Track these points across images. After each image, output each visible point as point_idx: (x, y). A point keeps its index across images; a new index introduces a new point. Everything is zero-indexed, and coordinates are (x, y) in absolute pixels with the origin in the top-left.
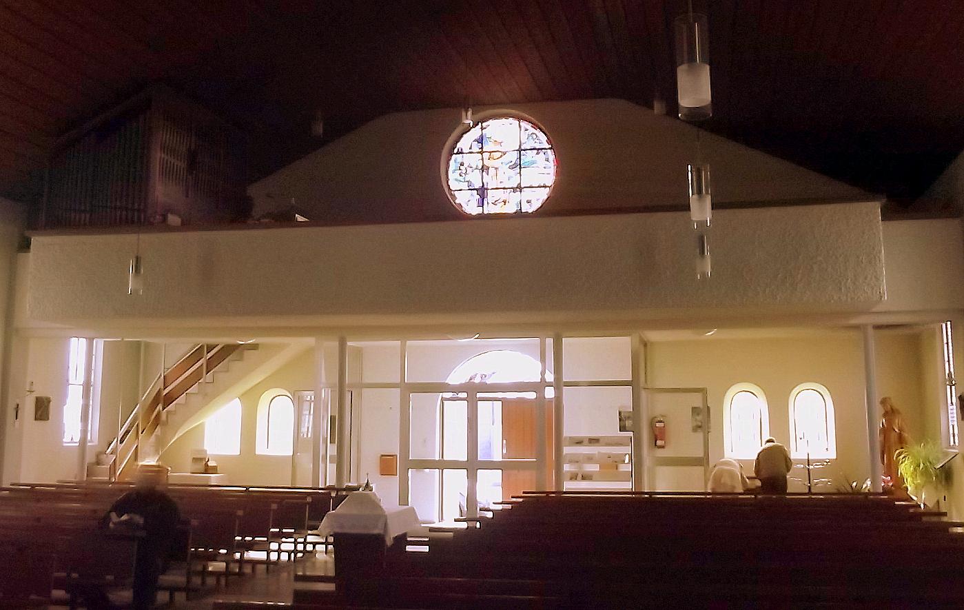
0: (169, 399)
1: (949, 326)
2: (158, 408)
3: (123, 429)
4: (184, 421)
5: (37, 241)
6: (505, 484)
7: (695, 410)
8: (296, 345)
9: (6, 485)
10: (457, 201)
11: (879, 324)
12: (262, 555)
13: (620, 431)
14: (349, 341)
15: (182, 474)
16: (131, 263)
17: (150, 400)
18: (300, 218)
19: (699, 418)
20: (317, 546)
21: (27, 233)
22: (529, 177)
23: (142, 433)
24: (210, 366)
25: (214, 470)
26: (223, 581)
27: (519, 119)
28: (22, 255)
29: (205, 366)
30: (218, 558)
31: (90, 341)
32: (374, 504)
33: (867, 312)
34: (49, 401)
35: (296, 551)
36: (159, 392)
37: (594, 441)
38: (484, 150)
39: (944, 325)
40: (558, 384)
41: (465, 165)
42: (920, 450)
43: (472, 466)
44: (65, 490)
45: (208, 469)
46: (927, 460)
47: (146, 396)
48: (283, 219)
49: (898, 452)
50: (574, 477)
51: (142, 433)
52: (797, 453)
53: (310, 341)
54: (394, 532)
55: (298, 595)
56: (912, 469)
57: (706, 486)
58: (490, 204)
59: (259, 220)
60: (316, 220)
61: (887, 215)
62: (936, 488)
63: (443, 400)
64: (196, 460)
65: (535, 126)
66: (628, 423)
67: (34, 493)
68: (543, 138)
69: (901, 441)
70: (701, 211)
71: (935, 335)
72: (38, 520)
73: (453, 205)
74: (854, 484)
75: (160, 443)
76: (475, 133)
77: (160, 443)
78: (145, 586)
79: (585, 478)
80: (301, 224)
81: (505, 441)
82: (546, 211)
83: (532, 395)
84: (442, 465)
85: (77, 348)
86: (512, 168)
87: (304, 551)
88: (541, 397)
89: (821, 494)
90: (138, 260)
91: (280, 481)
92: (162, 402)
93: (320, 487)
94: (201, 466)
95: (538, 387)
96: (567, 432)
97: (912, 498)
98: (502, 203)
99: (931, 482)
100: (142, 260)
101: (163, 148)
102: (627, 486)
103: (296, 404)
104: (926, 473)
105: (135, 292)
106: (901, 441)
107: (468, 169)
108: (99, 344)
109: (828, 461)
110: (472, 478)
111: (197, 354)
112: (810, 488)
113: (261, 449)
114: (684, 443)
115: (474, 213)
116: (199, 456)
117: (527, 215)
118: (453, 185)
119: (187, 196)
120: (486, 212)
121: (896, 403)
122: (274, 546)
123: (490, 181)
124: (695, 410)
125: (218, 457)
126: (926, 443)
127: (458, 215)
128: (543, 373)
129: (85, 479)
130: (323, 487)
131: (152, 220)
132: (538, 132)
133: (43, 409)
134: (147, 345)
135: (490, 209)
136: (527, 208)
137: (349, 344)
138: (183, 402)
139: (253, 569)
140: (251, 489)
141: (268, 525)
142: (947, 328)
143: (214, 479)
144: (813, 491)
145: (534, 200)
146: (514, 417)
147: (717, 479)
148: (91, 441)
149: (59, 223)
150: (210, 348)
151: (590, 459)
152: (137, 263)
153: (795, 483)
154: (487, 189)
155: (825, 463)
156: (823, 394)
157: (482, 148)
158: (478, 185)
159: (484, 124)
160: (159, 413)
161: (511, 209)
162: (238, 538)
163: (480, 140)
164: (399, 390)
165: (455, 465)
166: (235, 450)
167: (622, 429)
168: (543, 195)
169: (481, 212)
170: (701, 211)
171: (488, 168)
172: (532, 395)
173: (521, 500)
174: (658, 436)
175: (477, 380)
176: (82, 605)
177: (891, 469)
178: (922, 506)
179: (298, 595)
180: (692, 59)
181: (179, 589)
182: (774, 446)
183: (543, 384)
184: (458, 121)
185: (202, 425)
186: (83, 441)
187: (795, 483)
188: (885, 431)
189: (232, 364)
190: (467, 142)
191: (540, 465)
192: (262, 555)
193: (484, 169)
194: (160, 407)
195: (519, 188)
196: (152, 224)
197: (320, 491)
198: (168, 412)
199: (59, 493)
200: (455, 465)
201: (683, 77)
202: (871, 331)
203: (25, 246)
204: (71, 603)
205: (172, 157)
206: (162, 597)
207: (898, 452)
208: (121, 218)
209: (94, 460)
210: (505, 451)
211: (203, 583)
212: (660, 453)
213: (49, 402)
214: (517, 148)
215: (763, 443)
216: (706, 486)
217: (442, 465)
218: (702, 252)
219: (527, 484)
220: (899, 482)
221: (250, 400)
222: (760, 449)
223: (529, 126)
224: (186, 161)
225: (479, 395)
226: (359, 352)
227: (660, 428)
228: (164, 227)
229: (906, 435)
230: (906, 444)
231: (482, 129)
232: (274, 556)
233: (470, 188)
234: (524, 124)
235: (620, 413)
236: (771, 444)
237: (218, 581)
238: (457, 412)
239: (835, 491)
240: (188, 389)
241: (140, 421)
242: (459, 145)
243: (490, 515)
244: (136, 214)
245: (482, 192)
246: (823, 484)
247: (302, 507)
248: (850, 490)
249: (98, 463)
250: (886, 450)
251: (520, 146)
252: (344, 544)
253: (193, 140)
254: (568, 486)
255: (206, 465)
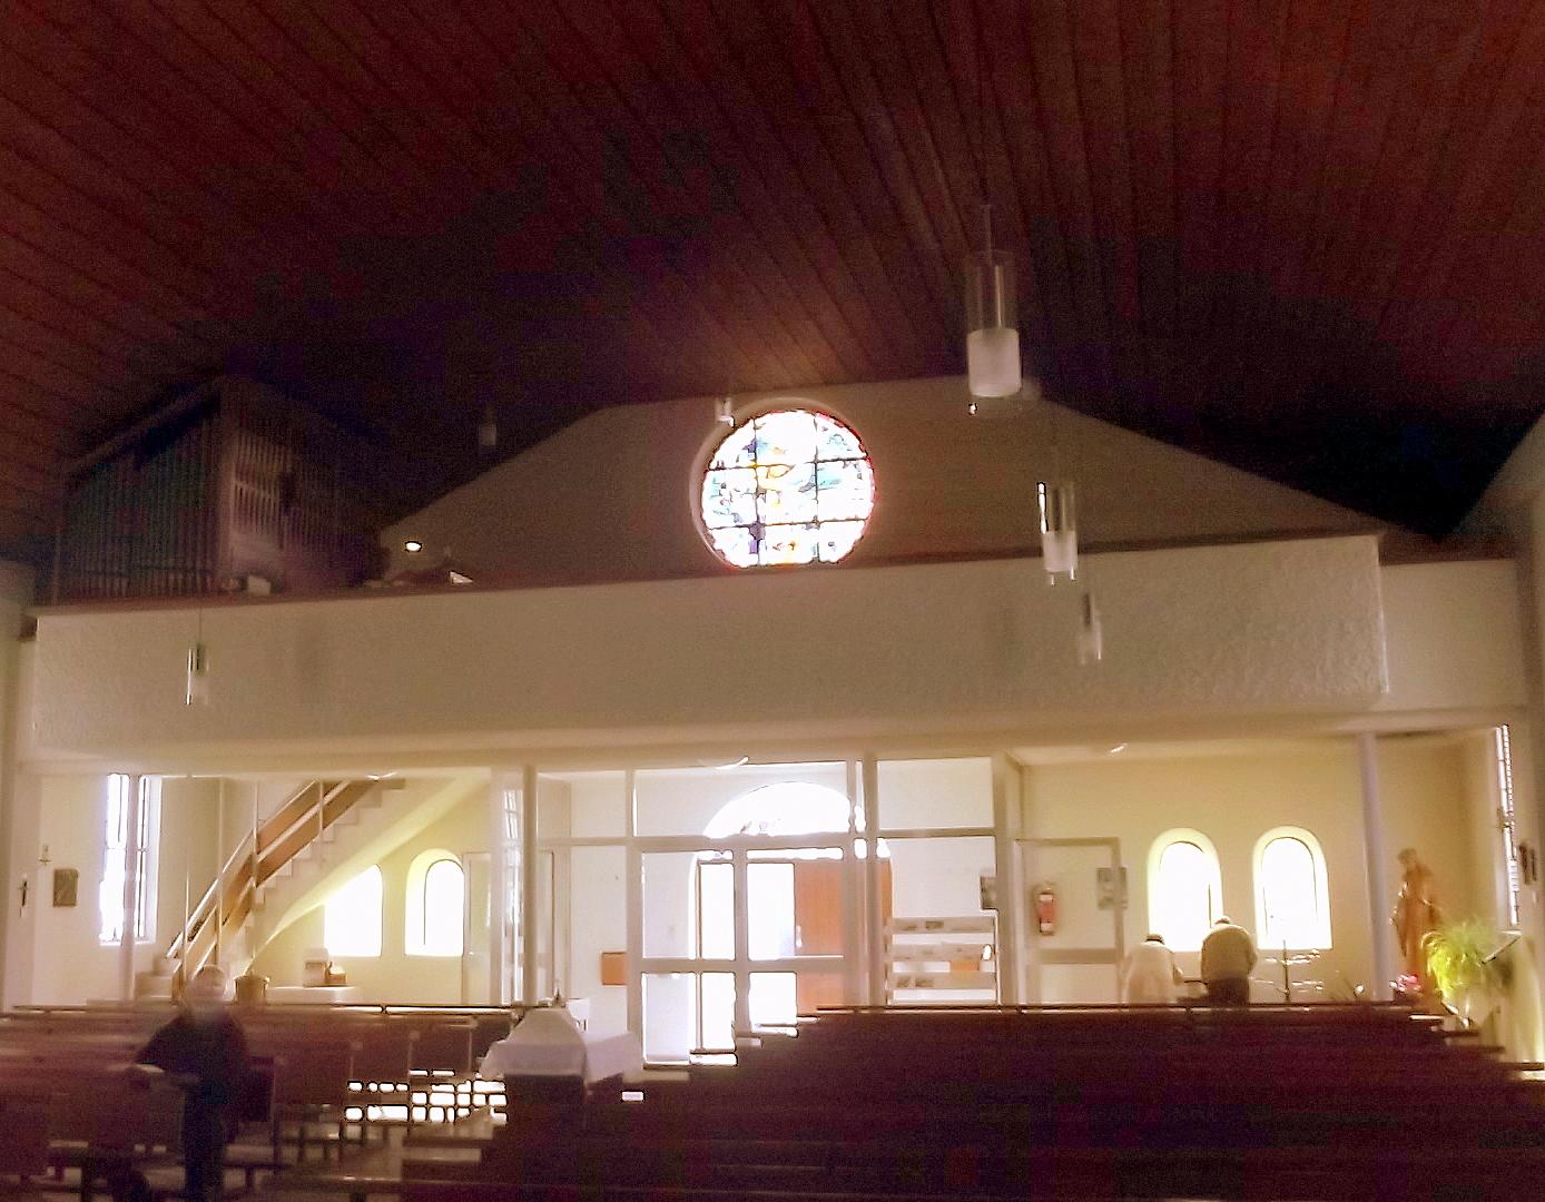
0: (266, 870)
1: (1506, 733)
2: (248, 885)
3: (192, 918)
4: (289, 906)
5: (46, 623)
6: (802, 991)
7: (1103, 875)
8: (464, 779)
9: (7, 1009)
10: (716, 546)
11: (1408, 730)
12: (398, 1113)
13: (984, 909)
14: (541, 771)
15: (288, 987)
16: (191, 655)
17: (236, 872)
18: (457, 579)
19: (1109, 886)
20: (491, 1097)
21: (32, 612)
22: (828, 505)
23: (224, 923)
24: (329, 814)
25: (339, 981)
26: (334, 1154)
27: (814, 411)
28: (25, 647)
29: (321, 815)
30: (321, 1117)
31: (135, 779)
32: (567, 1028)
33: (1363, 713)
34: (75, 875)
35: (456, 1107)
36: (251, 857)
37: (934, 925)
38: (759, 463)
39: (1498, 731)
40: (872, 835)
41: (730, 487)
42: (1461, 932)
43: (741, 968)
44: (101, 1015)
45: (330, 980)
46: (1473, 949)
47: (229, 866)
48: (430, 579)
49: (1425, 936)
50: (903, 983)
51: (224, 923)
52: (1266, 940)
53: (481, 773)
54: (598, 1073)
55: (409, 1168)
56: (1448, 963)
57: (1120, 996)
58: (770, 548)
59: (389, 583)
60: (484, 579)
61: (1388, 557)
62: (1488, 993)
63: (700, 863)
64: (311, 965)
65: (840, 423)
66: (993, 897)
67: (49, 1021)
68: (853, 441)
69: (1433, 918)
70: (1061, 556)
71: (1485, 746)
72: (40, 1060)
73: (709, 551)
74: (1360, 989)
75: (253, 939)
76: (744, 435)
77: (253, 939)
78: (203, 1165)
79: (920, 984)
80: (460, 588)
81: (799, 928)
82: (861, 558)
83: (835, 854)
84: (701, 967)
85: (116, 787)
86: (803, 490)
87: (471, 1106)
88: (850, 857)
89: (1307, 1006)
90: (200, 652)
91: (443, 995)
92: (255, 868)
93: (503, 1003)
94: (320, 976)
95: (843, 841)
96: (898, 912)
97: (1449, 1011)
98: (788, 548)
99: (1479, 984)
100: (207, 651)
101: (241, 474)
102: (987, 996)
103: (467, 869)
104: (1469, 970)
105: (197, 700)
106: (1433, 918)
107: (734, 493)
108: (153, 787)
109: (1315, 952)
110: (742, 987)
111: (309, 798)
112: (1287, 995)
113: (413, 947)
114: (1085, 925)
115: (744, 565)
116: (316, 959)
117: (828, 566)
118: (711, 519)
119: (281, 546)
120: (763, 563)
121: (1424, 857)
122: (419, 1098)
123: (769, 512)
124: (1103, 875)
125: (345, 961)
126: (1472, 921)
127: (709, 566)
128: (852, 820)
129: (131, 996)
130: (508, 1004)
131: (223, 586)
132: (844, 432)
133: (65, 889)
134: (230, 785)
135: (768, 557)
136: (831, 555)
137: (541, 775)
138: (289, 873)
139: (385, 1136)
140: (389, 1009)
141: (406, 1066)
142: (1502, 735)
143: (339, 994)
144: (1294, 1000)
145: (839, 542)
146: (812, 888)
147: (1137, 986)
148: (145, 938)
149: (82, 594)
150: (329, 787)
151: (929, 954)
152: (198, 655)
153: (1263, 989)
154: (764, 525)
155: (1312, 956)
156: (1307, 843)
157: (755, 460)
158: (751, 520)
159: (759, 422)
160: (251, 889)
161: (802, 556)
162: (356, 1087)
163: (752, 448)
164: (622, 849)
165: (717, 967)
166: (373, 950)
167: (986, 905)
168: (855, 532)
169: (754, 562)
170: (1061, 556)
171: (765, 493)
172: (835, 854)
173: (813, 1019)
174: (1043, 915)
175: (753, 832)
176: (101, 1191)
177: (1416, 964)
178: (1466, 1022)
179: (409, 1168)
180: (989, 322)
181: (262, 1166)
182: (1227, 929)
183: (853, 834)
184: (709, 420)
185: (318, 912)
186: (128, 937)
187: (1263, 989)
188: (1408, 904)
189: (364, 811)
190: (731, 450)
191: (848, 966)
192: (398, 1113)
193: (760, 493)
194: (252, 882)
195: (816, 523)
196: (221, 592)
197: (503, 1011)
198: (267, 891)
199: (89, 1020)
200: (717, 967)
201: (976, 345)
202: (1371, 744)
203: (28, 631)
204: (85, 1190)
205: (256, 484)
206: (233, 1179)
207: (1425, 936)
208: (112, 591)
209: (149, 968)
210: (799, 943)
211: (301, 1155)
212: (1050, 943)
213: (77, 876)
214: (812, 459)
215: (1213, 925)
216: (1120, 996)
217: (701, 967)
218: (1088, 621)
219: (834, 995)
220: (1429, 984)
221: (396, 868)
222: (1207, 932)
223: (830, 423)
224: (278, 491)
225: (752, 855)
226: (564, 791)
227: (1046, 904)
228: (241, 594)
229: (1440, 909)
230: (1441, 923)
231: (755, 429)
232: (419, 1114)
233: (738, 524)
234: (821, 420)
235: (982, 879)
236: (1225, 926)
237: (326, 1153)
238: (719, 879)
239: (1330, 1000)
240: (296, 852)
241: (220, 905)
242: (719, 456)
243: (757, 1043)
244: (101, 578)
245: (757, 529)
246: (1309, 989)
247: (460, 1036)
248: (1352, 999)
249: (157, 972)
250: (1408, 931)
251: (816, 456)
252: (517, 1088)
253: (289, 457)
254: (902, 997)
255: (328, 973)
